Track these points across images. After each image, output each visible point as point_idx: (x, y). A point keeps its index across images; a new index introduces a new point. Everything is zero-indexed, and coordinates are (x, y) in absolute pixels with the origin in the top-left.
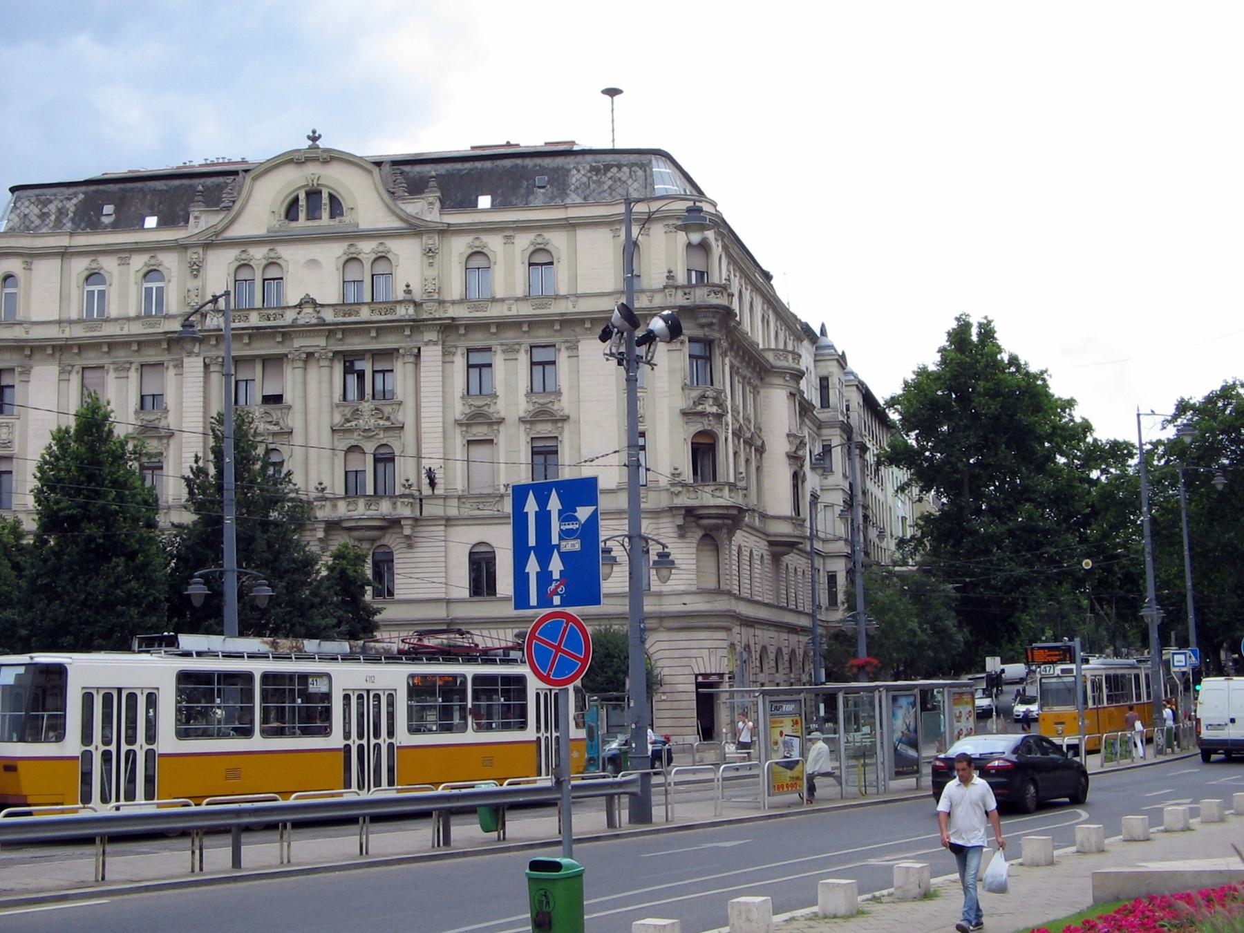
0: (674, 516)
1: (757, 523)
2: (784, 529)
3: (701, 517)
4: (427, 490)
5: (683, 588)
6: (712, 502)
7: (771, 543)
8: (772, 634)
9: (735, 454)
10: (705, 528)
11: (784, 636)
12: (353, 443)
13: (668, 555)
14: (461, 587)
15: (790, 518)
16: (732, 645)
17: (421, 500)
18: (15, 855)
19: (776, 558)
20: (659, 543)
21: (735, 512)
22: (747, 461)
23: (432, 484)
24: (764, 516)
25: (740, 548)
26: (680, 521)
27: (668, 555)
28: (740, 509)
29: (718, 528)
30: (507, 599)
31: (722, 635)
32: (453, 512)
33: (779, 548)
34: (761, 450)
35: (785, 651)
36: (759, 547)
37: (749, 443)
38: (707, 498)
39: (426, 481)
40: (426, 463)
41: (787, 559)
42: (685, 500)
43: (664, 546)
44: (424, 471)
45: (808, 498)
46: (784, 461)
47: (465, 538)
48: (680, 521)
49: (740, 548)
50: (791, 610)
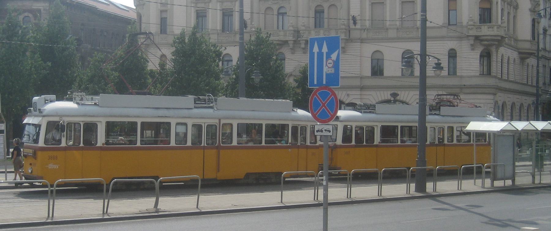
0: (469, 40)
1: (513, 43)
2: (527, 46)
3: (482, 40)
4: (352, 26)
5: (472, 74)
6: (488, 33)
7: (520, 53)
8: (518, 97)
9: (502, 10)
10: (484, 45)
11: (524, 98)
12: (319, 4)
13: (440, 64)
14: (368, 72)
15: (531, 41)
16: (496, 102)
17: (349, 31)
18: (125, 216)
19: (523, 59)
20: (436, 58)
21: (499, 38)
22: (509, 13)
23: (355, 23)
24: (516, 40)
25: (502, 55)
26: (472, 42)
27: (440, 64)
28: (502, 37)
29: (491, 45)
30: (417, 77)
31: (491, 97)
32: (364, 35)
33: (524, 56)
34: (516, 7)
35: (508, 103)
36: (514, 55)
37: (510, 4)
38: (485, 31)
39: (352, 22)
40: (352, 13)
41: (528, 61)
42: (473, 32)
43: (438, 60)
44: (351, 17)
45: (541, 31)
46: (528, 13)
47: (369, 49)
48: (472, 42)
49: (502, 55)
50: (529, 85)
